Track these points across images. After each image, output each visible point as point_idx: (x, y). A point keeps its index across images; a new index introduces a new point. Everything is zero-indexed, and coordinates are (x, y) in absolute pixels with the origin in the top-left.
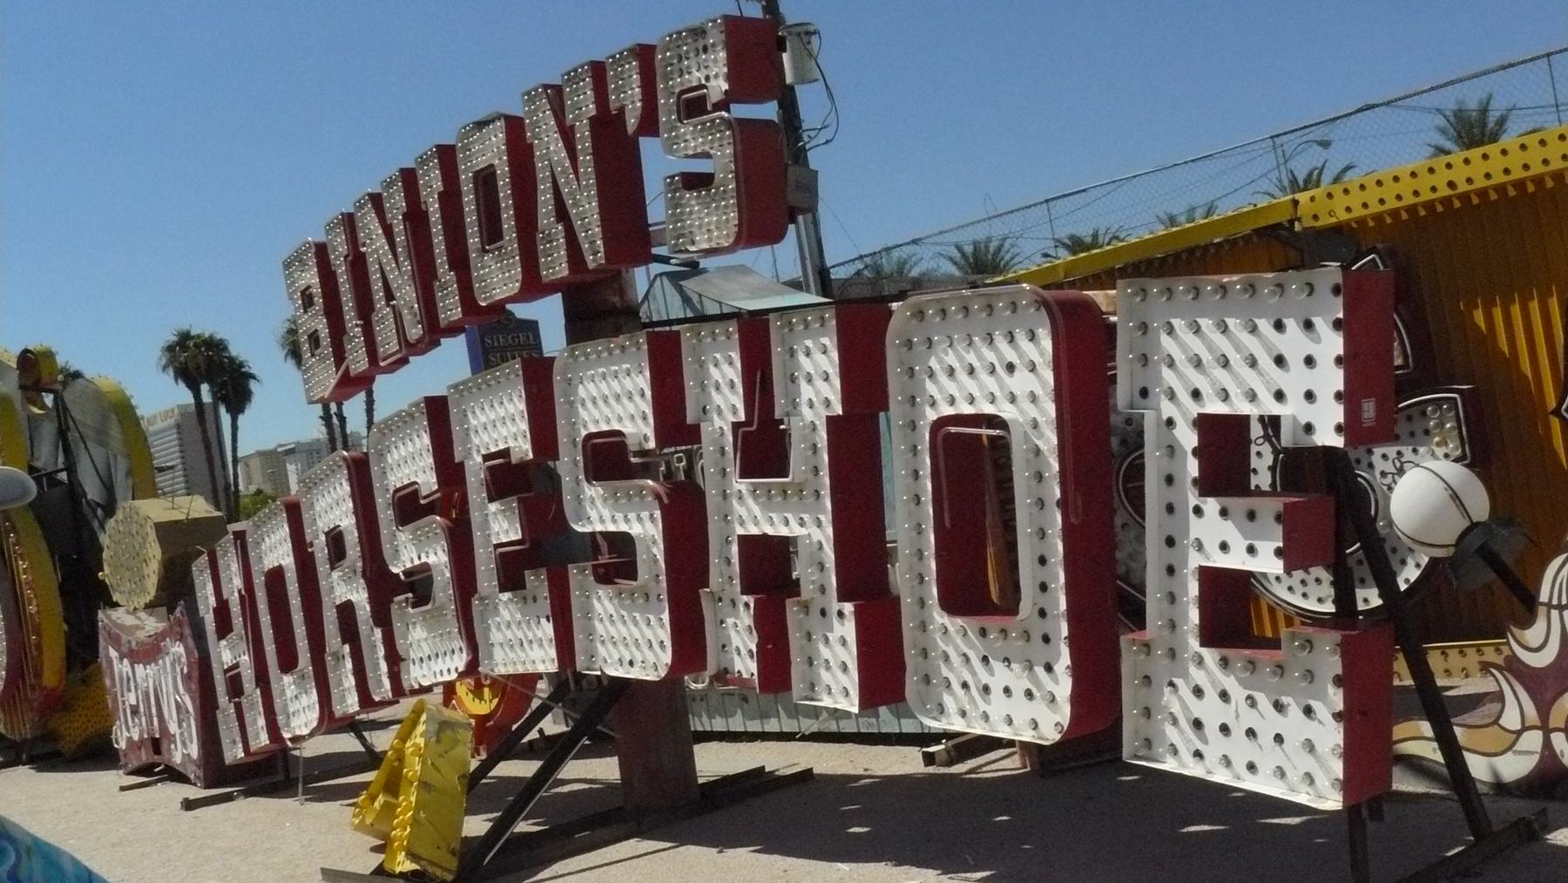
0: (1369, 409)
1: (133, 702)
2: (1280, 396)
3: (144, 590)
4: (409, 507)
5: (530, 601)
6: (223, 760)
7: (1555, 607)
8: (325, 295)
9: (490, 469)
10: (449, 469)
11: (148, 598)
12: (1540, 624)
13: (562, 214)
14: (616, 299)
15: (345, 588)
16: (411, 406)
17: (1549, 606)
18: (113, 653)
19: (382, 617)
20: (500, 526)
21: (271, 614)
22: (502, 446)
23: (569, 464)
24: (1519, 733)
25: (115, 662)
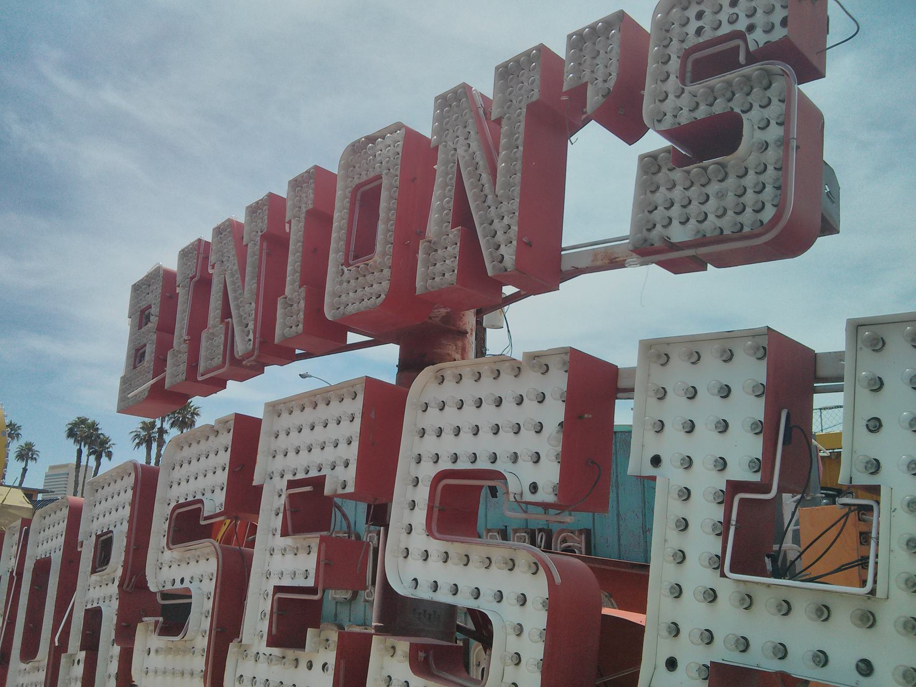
4: (188, 526)
5: (303, 665)
8: (161, 316)
10: (244, 495)
13: (462, 216)
15: (99, 591)
16: (219, 421)
19: (125, 635)
20: (283, 561)
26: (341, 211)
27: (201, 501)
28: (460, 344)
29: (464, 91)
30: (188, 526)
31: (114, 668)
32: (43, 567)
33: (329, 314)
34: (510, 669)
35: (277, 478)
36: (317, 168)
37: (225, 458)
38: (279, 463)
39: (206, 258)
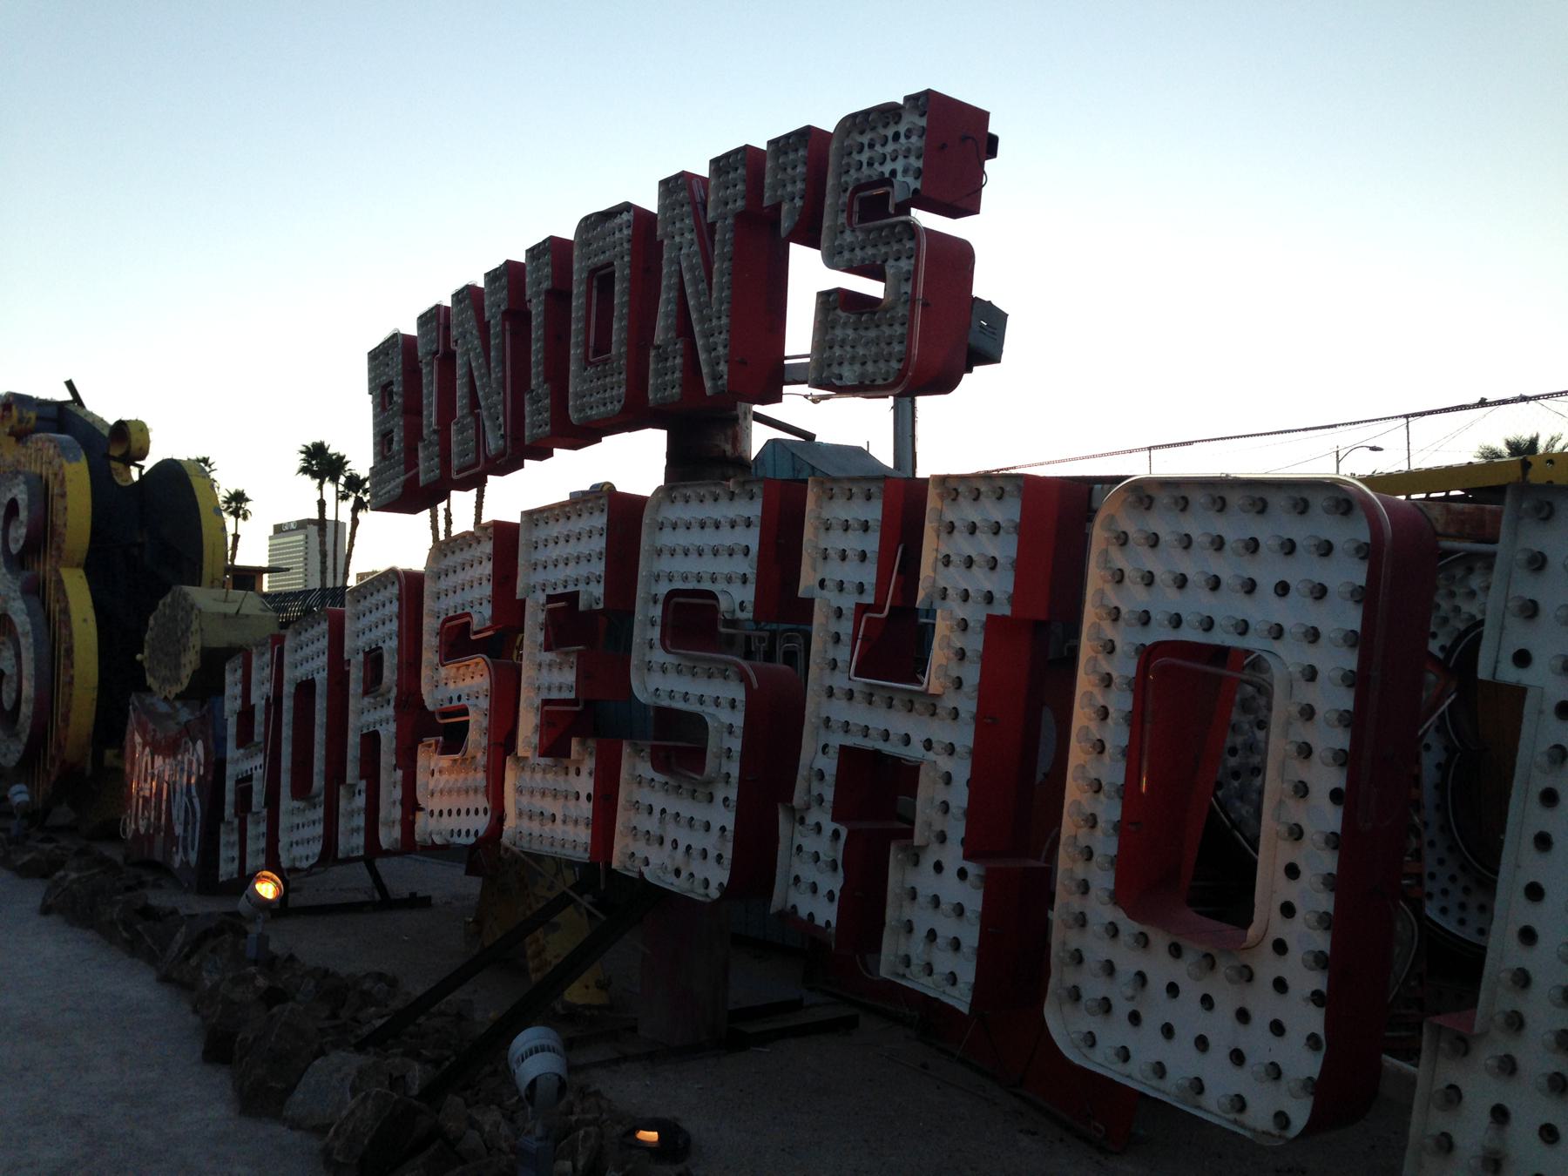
1: (147, 793)
3: (178, 680)
4: (458, 641)
5: (572, 771)
6: (217, 876)
9: (550, 611)
11: (178, 689)
13: (684, 327)
14: (728, 448)
15: (371, 715)
18: (138, 739)
20: (546, 676)
21: (294, 730)
22: (571, 588)
23: (647, 618)
25: (139, 749)
26: (430, 364)
27: (469, 614)
30: (458, 642)
31: (398, 793)
33: (574, 417)
35: (539, 592)
36: (551, 238)
37: (488, 568)
38: (539, 577)
39: (447, 328)
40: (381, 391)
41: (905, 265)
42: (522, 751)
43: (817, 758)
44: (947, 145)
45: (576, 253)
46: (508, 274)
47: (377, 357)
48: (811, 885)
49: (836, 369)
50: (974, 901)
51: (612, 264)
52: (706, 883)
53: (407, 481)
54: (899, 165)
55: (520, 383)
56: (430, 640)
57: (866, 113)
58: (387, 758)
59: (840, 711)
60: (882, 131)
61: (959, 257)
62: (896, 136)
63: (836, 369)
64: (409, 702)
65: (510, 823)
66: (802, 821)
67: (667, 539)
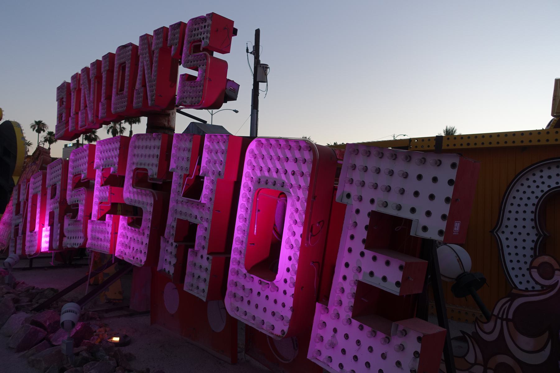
0: (457, 226)
2: (413, 210)
7: (500, 318)
12: (492, 324)
13: (144, 85)
14: (166, 124)
17: (497, 317)
20: (100, 193)
24: (473, 365)
26: (74, 92)
28: (167, 119)
29: (147, 35)
32: (35, 197)
34: (347, 185)
36: (109, 53)
40: (60, 100)
41: (204, 67)
42: (93, 218)
43: (171, 221)
44: (220, 31)
45: (116, 58)
46: (97, 64)
47: (59, 89)
48: (167, 263)
49: (185, 100)
50: (209, 267)
51: (125, 63)
52: (141, 261)
53: (65, 131)
54: (205, 36)
55: (99, 100)
56: (70, 181)
57: (196, 18)
58: (56, 219)
59: (180, 208)
60: (201, 25)
61: (224, 65)
62: (205, 27)
63: (185, 100)
64: (63, 202)
65: (89, 241)
66: (168, 242)
67: (136, 152)
